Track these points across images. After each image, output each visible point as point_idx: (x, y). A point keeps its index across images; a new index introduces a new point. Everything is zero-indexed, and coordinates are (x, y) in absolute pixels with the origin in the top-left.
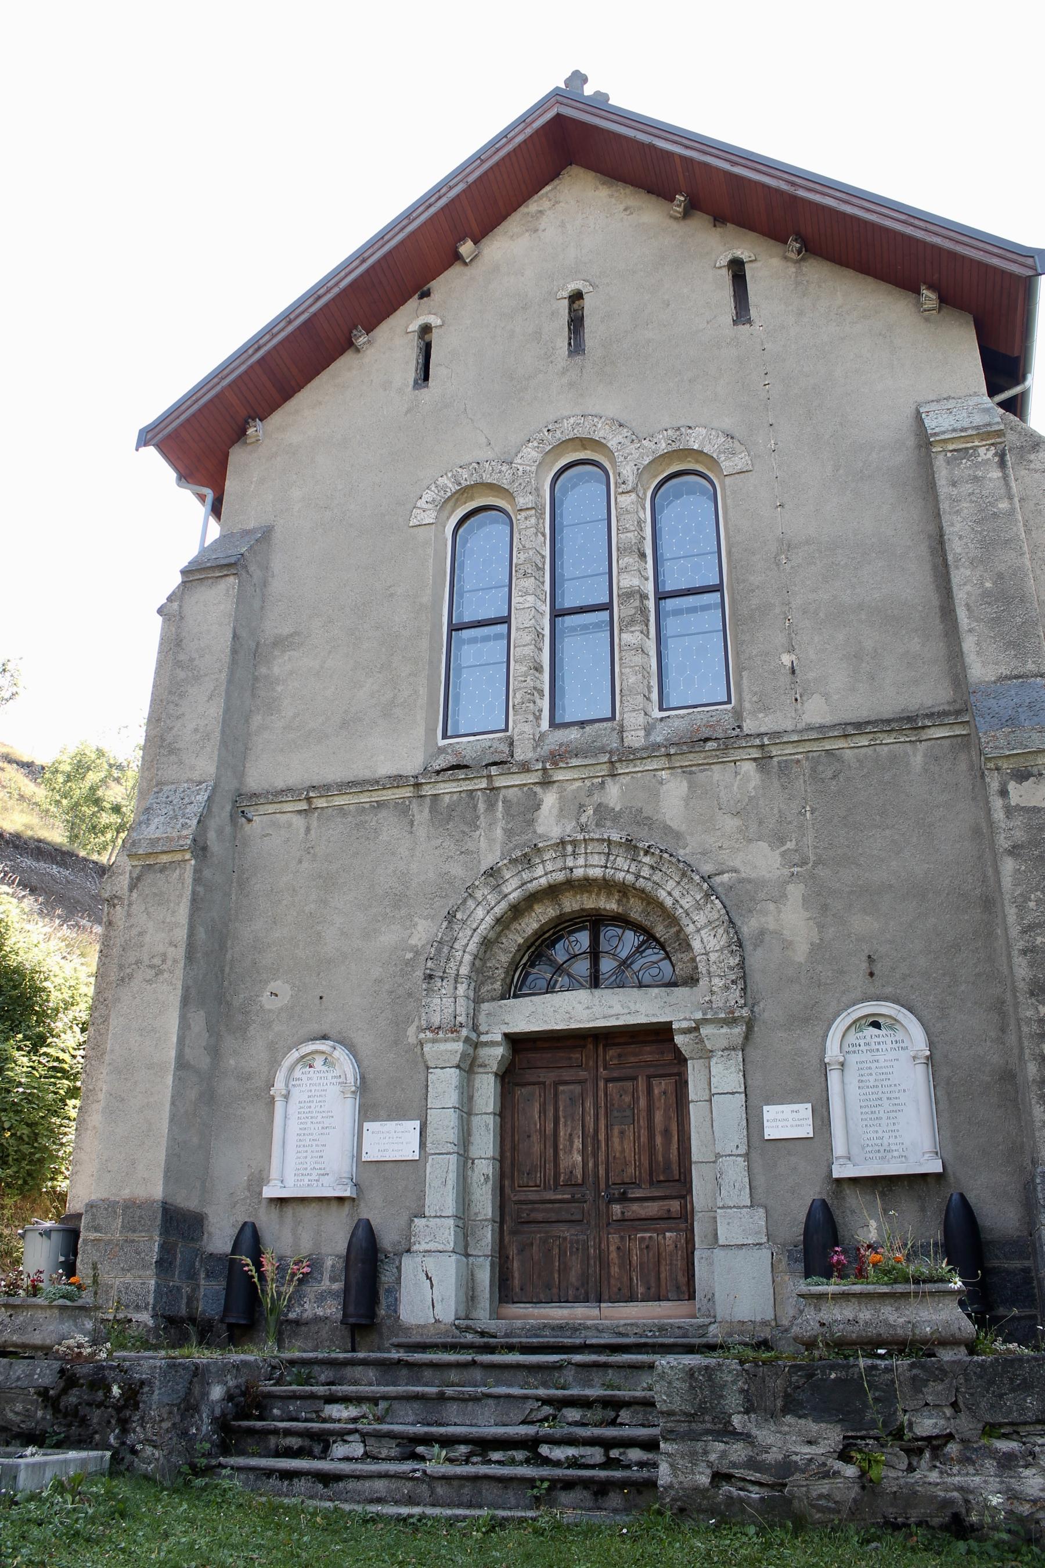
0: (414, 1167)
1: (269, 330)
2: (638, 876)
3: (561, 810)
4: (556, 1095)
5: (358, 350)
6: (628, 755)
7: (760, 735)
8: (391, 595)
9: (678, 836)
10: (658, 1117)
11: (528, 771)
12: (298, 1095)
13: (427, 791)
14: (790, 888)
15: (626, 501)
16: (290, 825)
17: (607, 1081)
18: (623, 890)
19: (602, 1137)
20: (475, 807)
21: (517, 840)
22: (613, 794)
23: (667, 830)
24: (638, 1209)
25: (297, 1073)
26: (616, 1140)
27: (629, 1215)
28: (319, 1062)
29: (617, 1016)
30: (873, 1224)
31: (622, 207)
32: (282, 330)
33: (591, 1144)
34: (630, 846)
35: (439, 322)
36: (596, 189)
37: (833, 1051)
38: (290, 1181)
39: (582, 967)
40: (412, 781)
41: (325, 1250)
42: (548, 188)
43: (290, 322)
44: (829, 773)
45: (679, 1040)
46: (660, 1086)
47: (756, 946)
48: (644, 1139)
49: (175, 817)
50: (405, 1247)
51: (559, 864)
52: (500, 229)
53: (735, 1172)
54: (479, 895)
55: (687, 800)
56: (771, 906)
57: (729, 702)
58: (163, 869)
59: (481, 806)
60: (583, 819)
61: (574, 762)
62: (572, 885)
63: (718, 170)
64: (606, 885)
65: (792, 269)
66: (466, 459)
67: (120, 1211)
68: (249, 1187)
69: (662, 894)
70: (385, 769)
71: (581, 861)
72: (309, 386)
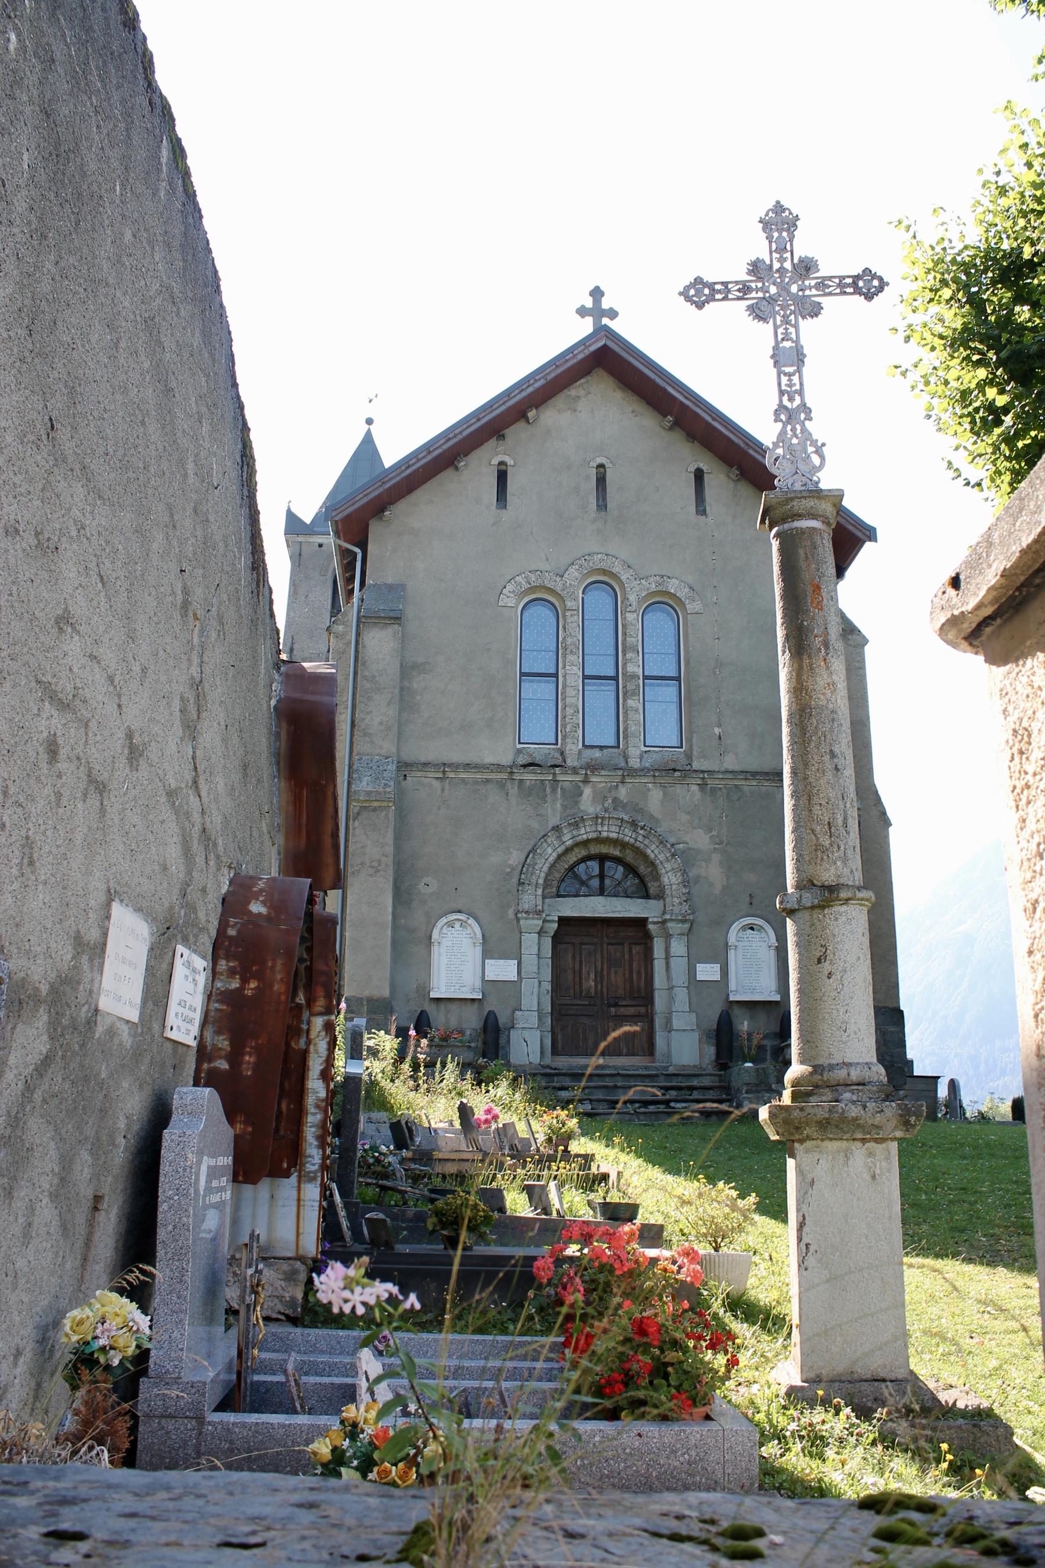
0: (516, 985)
1: (415, 455)
2: (636, 840)
3: (594, 798)
4: (581, 949)
5: (457, 469)
6: (633, 772)
7: (703, 772)
8: (489, 650)
9: (657, 821)
10: (635, 965)
11: (577, 774)
12: (446, 943)
13: (517, 777)
14: (714, 855)
15: (630, 617)
16: (431, 785)
17: (609, 944)
18: (623, 845)
19: (605, 973)
20: (545, 790)
21: (568, 812)
22: (623, 793)
23: (651, 817)
24: (622, 1011)
25: (445, 930)
26: (613, 975)
27: (619, 1013)
28: (457, 925)
29: (620, 912)
30: (746, 1023)
31: (631, 409)
32: (424, 457)
33: (599, 976)
34: (634, 824)
35: (512, 463)
36: (614, 391)
37: (732, 938)
38: (443, 989)
39: (595, 883)
40: (509, 770)
41: (464, 1026)
42: (582, 381)
43: (429, 453)
44: (736, 797)
45: (651, 927)
46: (636, 949)
47: (695, 884)
48: (627, 975)
49: (377, 778)
50: (510, 1025)
51: (594, 829)
52: (550, 402)
53: (681, 995)
54: (549, 840)
55: (662, 802)
56: (704, 864)
57: (681, 747)
58: (374, 810)
59: (548, 790)
60: (606, 805)
61: (603, 773)
62: (599, 840)
63: (703, 419)
64: (615, 842)
65: (732, 485)
66: (533, 567)
67: (365, 1003)
68: (417, 992)
69: (649, 851)
70: (489, 759)
71: (605, 828)
72: (424, 486)
